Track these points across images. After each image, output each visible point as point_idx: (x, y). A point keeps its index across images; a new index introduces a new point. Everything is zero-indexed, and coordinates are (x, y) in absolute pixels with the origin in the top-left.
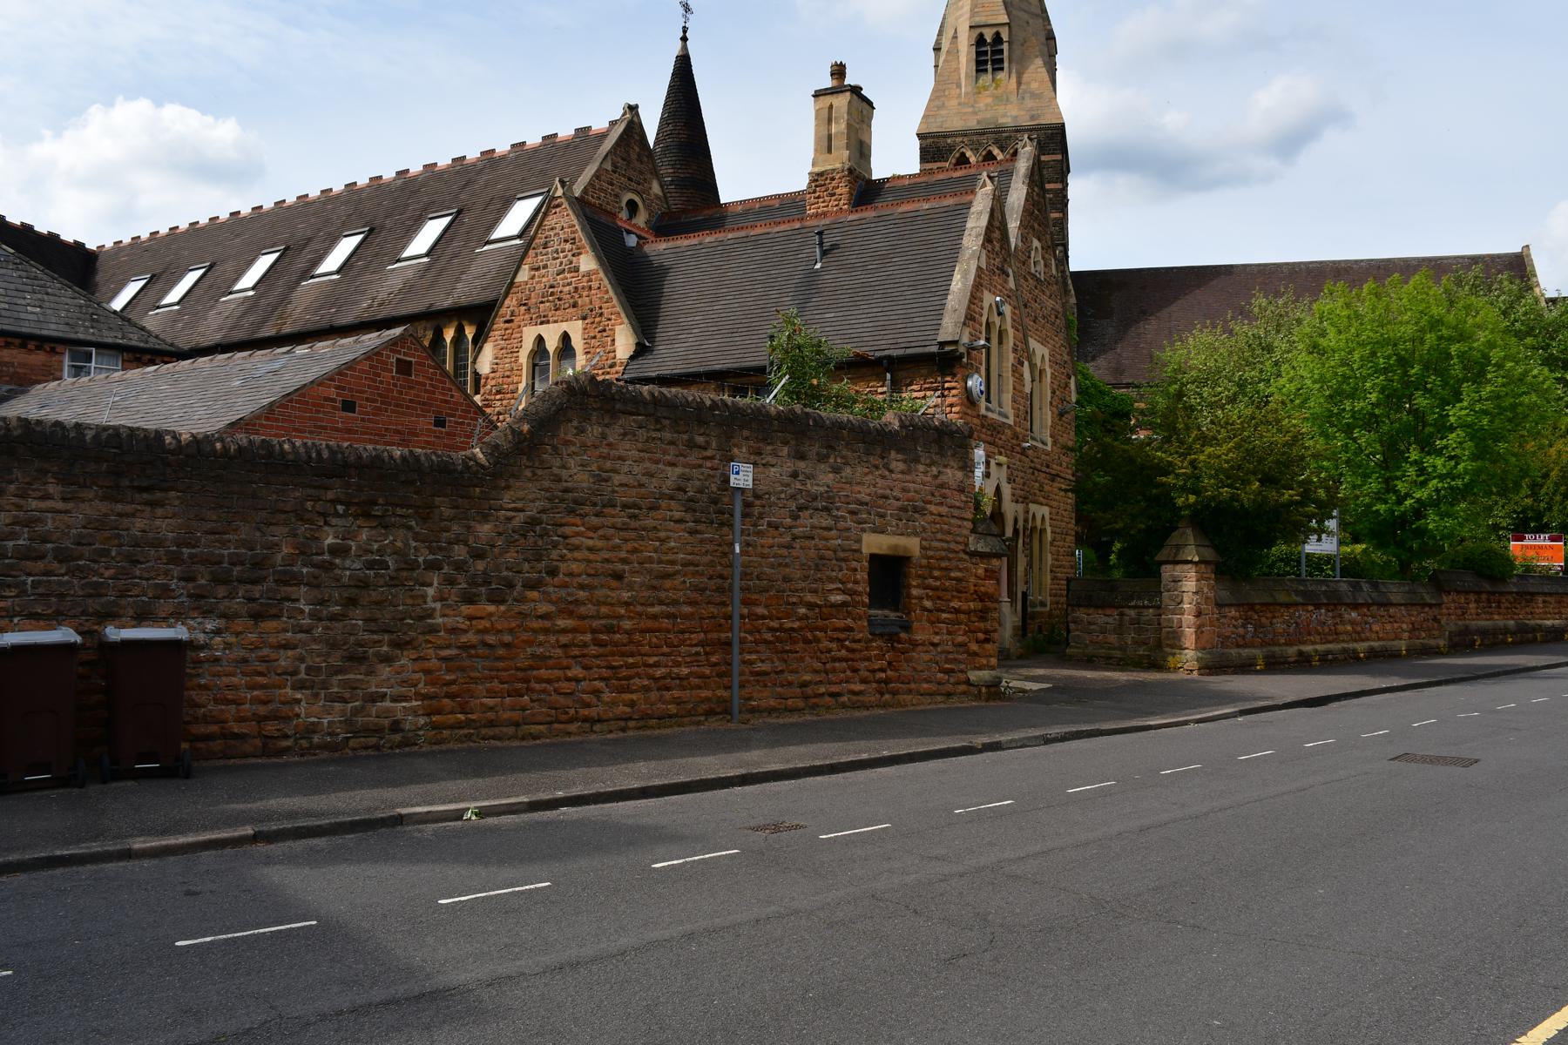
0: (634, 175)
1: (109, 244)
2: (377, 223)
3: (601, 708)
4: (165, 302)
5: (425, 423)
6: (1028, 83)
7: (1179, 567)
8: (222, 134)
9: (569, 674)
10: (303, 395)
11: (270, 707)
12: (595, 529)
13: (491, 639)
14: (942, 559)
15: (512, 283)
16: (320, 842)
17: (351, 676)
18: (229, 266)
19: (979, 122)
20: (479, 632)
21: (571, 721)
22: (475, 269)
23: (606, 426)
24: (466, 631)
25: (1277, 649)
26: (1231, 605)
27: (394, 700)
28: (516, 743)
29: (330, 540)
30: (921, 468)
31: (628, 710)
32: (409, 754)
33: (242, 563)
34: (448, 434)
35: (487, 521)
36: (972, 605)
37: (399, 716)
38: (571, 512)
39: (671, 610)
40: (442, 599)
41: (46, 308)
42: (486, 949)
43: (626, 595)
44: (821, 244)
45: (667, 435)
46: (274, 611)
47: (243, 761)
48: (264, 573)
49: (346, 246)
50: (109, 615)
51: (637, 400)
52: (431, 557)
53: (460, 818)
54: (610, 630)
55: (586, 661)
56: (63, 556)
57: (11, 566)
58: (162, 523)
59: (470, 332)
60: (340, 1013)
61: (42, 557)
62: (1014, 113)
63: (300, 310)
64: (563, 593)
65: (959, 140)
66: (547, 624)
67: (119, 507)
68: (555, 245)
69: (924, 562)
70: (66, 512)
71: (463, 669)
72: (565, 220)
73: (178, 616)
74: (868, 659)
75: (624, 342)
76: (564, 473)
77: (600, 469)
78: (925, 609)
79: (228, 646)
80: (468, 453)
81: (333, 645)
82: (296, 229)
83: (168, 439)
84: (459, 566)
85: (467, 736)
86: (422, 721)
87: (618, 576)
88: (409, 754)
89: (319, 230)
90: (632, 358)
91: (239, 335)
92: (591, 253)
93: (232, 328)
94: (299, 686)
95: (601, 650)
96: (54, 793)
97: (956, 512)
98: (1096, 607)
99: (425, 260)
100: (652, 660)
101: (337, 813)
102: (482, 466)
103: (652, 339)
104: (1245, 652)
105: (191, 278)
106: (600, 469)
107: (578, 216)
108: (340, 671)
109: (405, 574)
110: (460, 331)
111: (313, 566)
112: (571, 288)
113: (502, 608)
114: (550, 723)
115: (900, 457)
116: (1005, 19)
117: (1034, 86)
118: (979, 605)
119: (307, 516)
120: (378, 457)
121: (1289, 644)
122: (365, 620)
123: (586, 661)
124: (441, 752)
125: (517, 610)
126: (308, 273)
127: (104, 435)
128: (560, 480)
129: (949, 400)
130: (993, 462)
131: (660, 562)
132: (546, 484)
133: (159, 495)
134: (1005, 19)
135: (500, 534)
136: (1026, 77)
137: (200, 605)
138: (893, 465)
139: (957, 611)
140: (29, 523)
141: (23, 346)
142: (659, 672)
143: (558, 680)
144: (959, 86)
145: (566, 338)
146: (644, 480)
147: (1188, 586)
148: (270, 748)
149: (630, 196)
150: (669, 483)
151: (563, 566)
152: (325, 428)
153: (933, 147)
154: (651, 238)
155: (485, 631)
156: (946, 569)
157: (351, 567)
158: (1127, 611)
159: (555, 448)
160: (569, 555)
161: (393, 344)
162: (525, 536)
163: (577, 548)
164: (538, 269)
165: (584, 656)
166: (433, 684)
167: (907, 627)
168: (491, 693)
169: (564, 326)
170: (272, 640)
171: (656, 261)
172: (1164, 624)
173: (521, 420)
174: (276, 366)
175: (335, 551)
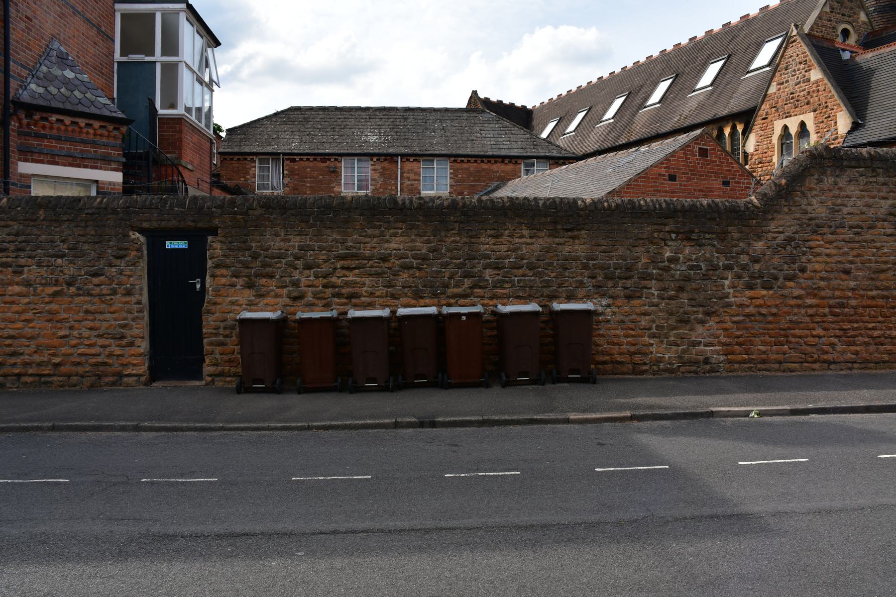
0: (844, 11)
1: (538, 105)
2: (680, 71)
3: (835, 355)
4: (567, 131)
5: (717, 184)
8: (589, 37)
9: (814, 333)
10: (646, 174)
11: (637, 347)
12: (831, 242)
13: (764, 311)
15: (766, 95)
16: (667, 423)
17: (681, 331)
18: (599, 108)
20: (756, 306)
21: (815, 362)
22: (742, 89)
23: (837, 176)
24: (748, 306)
27: (706, 346)
28: (779, 374)
29: (668, 254)
31: (854, 356)
32: (715, 377)
33: (620, 268)
34: (731, 190)
35: (761, 240)
37: (709, 355)
38: (815, 232)
39: (885, 293)
40: (734, 287)
41: (511, 142)
42: (769, 494)
43: (852, 284)
45: (881, 179)
46: (638, 294)
47: (622, 376)
48: (632, 273)
49: (663, 87)
50: (553, 297)
51: (859, 159)
52: (727, 262)
53: (747, 416)
54: (842, 306)
55: (825, 325)
56: (531, 267)
57: (507, 272)
58: (577, 248)
59: (740, 128)
60: (685, 518)
61: (521, 267)
63: (640, 127)
64: (810, 283)
66: (799, 302)
67: (557, 240)
68: (793, 67)
70: (532, 244)
71: (747, 329)
72: (800, 50)
73: (588, 297)
75: (843, 122)
76: (809, 209)
77: (834, 204)
79: (614, 313)
80: (747, 199)
81: (671, 314)
82: (633, 82)
83: (580, 202)
84: (744, 268)
85: (748, 368)
86: (722, 358)
87: (847, 272)
88: (715, 377)
89: (647, 80)
90: (849, 133)
91: (607, 145)
92: (818, 69)
93: (603, 141)
94: (653, 336)
95: (835, 319)
96: (530, 387)
99: (710, 88)
100: (871, 326)
101: (676, 408)
102: (757, 207)
103: (863, 118)
105: (580, 116)
106: (834, 204)
107: (808, 46)
108: (675, 328)
109: (711, 272)
110: (734, 128)
111: (659, 269)
112: (805, 93)
113: (771, 292)
114: (801, 362)
119: (656, 241)
120: (694, 205)
122: (689, 299)
123: (825, 325)
124: (734, 376)
125: (780, 293)
126: (642, 105)
127: (548, 203)
128: (807, 213)
131: (876, 262)
132: (798, 216)
133: (576, 233)
135: (769, 247)
137: (599, 291)
140: (514, 250)
141: (503, 162)
142: (876, 333)
143: (807, 336)
145: (803, 125)
146: (865, 209)
148: (636, 370)
150: (883, 210)
151: (810, 267)
152: (659, 191)
154: (860, 51)
155: (760, 306)
157: (680, 269)
159: (803, 193)
160: (814, 259)
161: (696, 139)
162: (784, 248)
163: (819, 255)
164: (782, 84)
165: (823, 322)
166: (729, 337)
168: (764, 343)
169: (801, 118)
170: (638, 310)
171: (865, 66)
173: (780, 177)
174: (630, 159)
175: (671, 260)
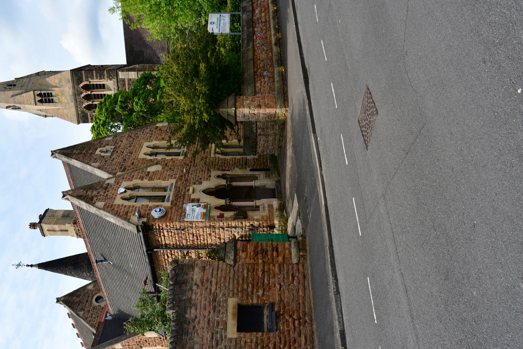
6: (56, 83)
7: (238, 115)
14: (238, 282)
19: (72, 102)
25: (274, 58)
26: (255, 86)
30: (194, 297)
36: (260, 261)
44: (101, 261)
62: (67, 89)
65: (79, 109)
69: (240, 295)
74: (289, 331)
78: (263, 294)
97: (215, 272)
98: (256, 144)
104: (277, 78)
115: (188, 311)
116: (32, 92)
117: (57, 81)
118: (260, 255)
121: (271, 49)
129: (164, 226)
130: (193, 197)
134: (32, 92)
136: (54, 84)
138: (193, 316)
139: (263, 271)
144: (59, 109)
147: (246, 111)
149: (94, 301)
153: (82, 119)
156: (243, 280)
158: (258, 133)
167: (273, 305)
172: (264, 120)
